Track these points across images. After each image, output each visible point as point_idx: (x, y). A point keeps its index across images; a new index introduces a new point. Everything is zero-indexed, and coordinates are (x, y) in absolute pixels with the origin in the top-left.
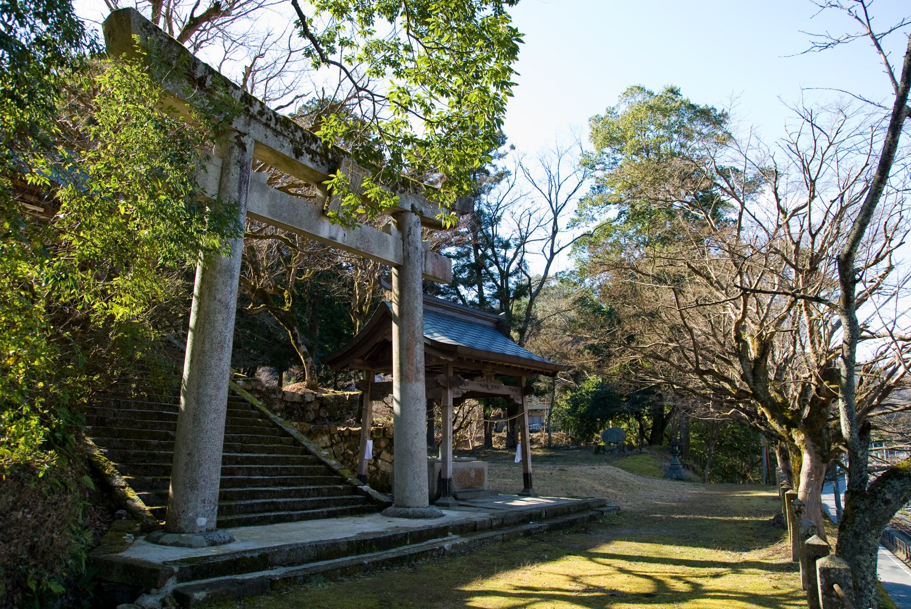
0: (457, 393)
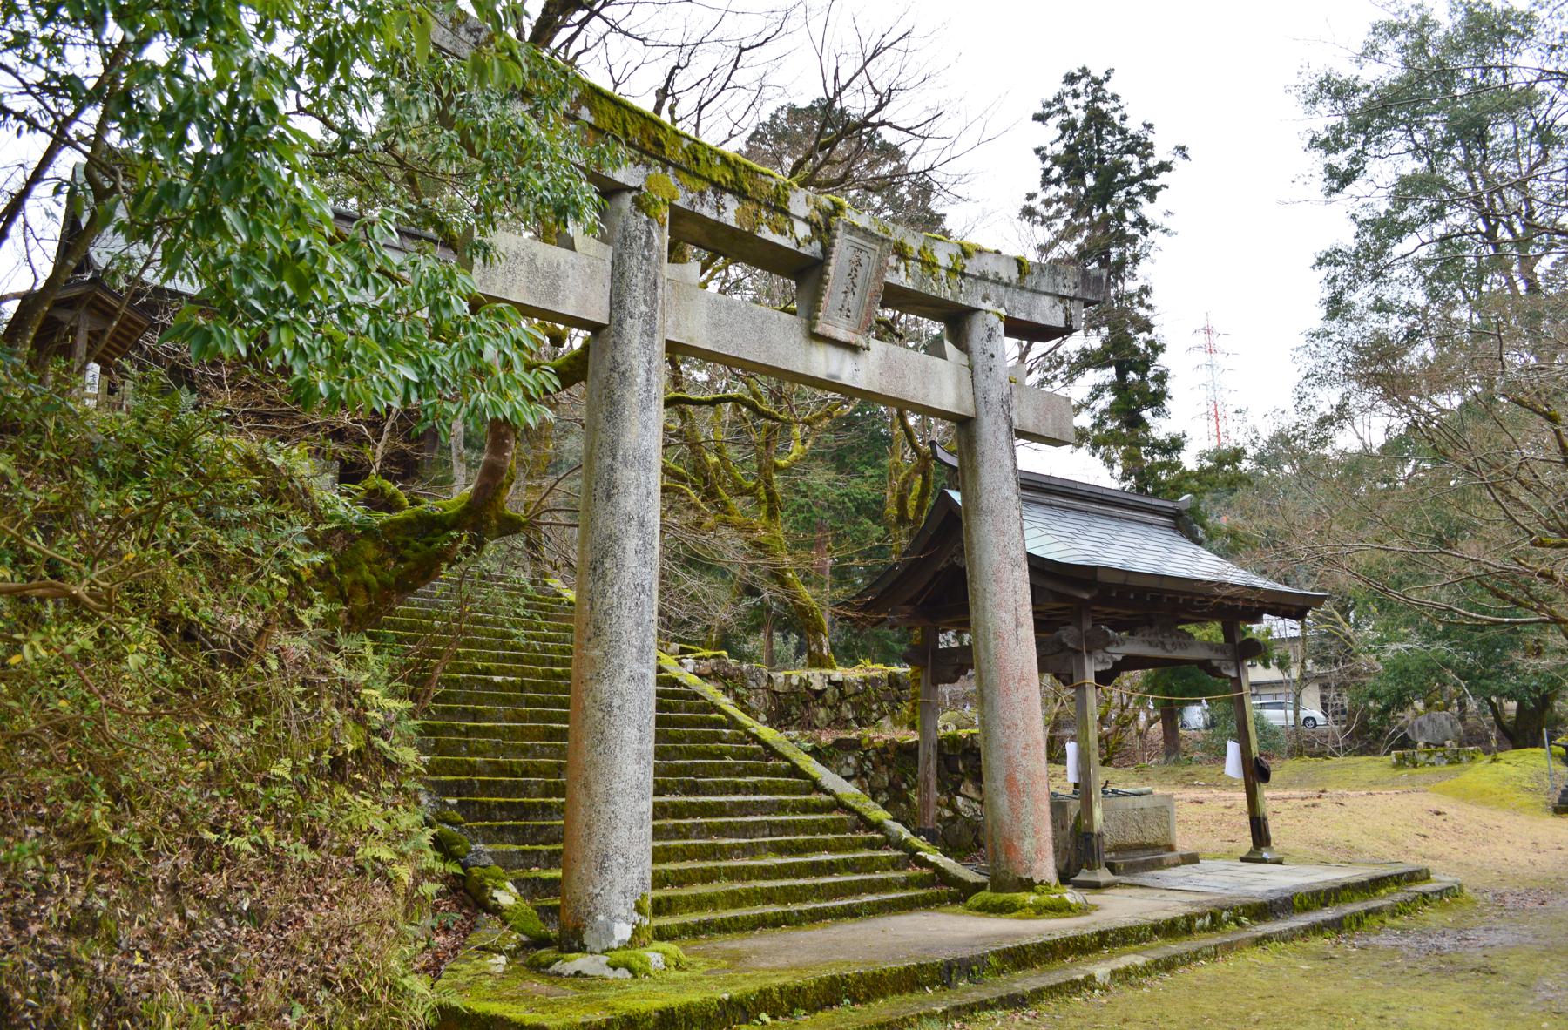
0: (1103, 662)
